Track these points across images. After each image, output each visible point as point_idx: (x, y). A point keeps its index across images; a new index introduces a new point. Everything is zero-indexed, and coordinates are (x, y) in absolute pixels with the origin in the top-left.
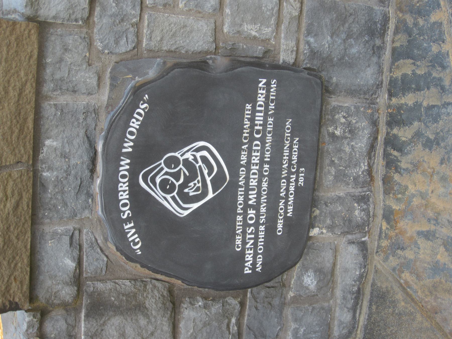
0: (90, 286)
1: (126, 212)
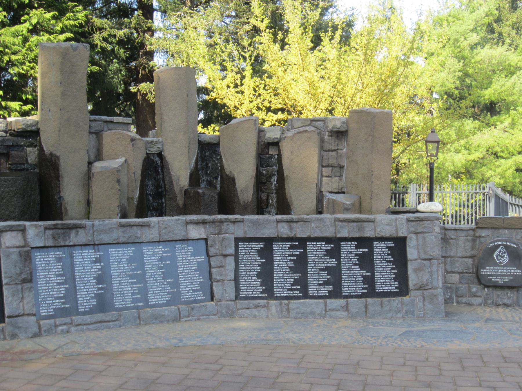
0: (478, 239)
1: (496, 244)
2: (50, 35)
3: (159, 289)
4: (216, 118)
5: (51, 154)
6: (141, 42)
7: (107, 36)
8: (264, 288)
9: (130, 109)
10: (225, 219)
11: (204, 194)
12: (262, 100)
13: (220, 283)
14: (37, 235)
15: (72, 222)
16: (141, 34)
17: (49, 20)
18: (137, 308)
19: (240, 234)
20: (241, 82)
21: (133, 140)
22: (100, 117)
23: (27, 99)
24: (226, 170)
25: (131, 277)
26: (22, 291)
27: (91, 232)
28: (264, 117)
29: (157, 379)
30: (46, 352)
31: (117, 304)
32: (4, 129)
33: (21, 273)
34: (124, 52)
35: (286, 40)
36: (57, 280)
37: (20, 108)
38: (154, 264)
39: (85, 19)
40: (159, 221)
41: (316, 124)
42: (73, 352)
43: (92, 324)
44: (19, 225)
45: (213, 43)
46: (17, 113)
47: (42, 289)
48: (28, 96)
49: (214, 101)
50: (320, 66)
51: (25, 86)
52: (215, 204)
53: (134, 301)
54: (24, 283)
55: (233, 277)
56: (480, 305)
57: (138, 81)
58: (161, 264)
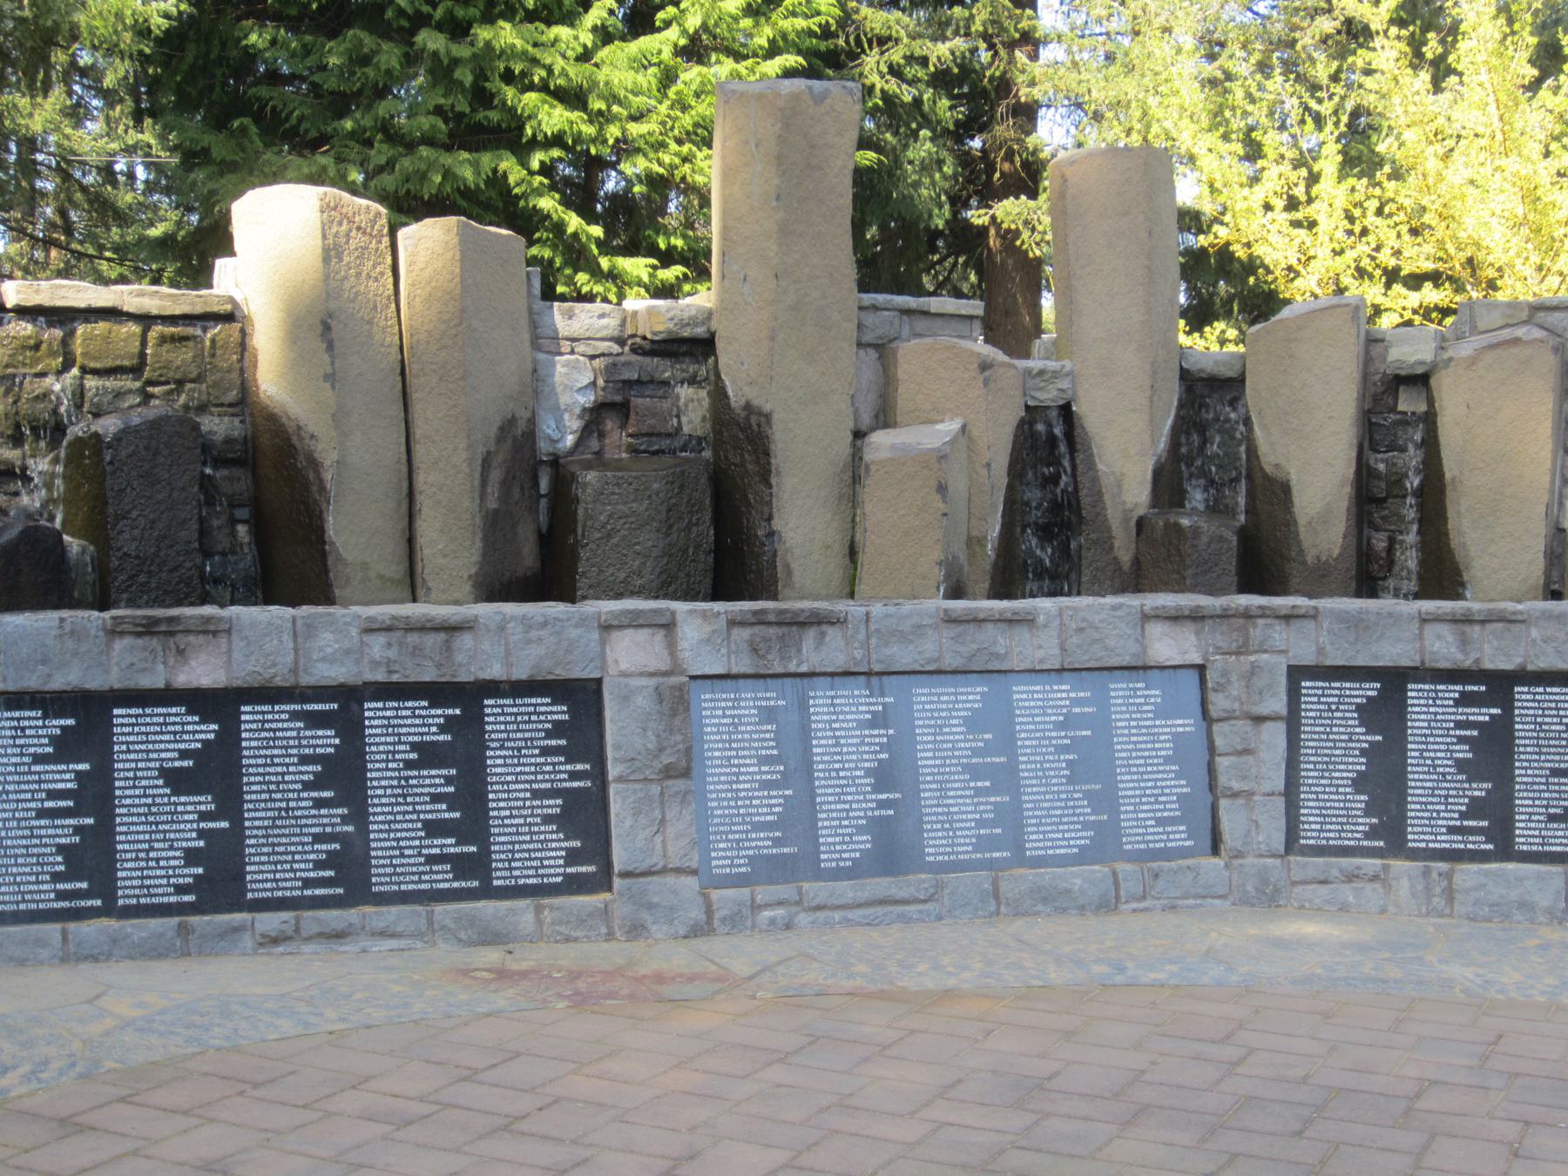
2: (737, 61)
3: (1059, 812)
4: (1223, 305)
5: (748, 407)
6: (1004, 73)
7: (902, 62)
8: (1375, 820)
9: (966, 279)
10: (1260, 607)
11: (1196, 531)
12: (1373, 245)
13: (1241, 801)
14: (708, 641)
15: (806, 605)
16: (1002, 52)
17: (736, 19)
18: (990, 865)
19: (1306, 655)
20: (1308, 193)
21: (985, 366)
22: (888, 297)
23: (671, 249)
24: (1263, 459)
25: (975, 772)
26: (662, 803)
27: (862, 636)
28: (1380, 300)
29: (1050, 1078)
30: (724, 981)
31: (931, 850)
32: (616, 333)
33: (661, 750)
34: (951, 108)
35: (1451, 59)
36: (760, 773)
37: (651, 276)
38: (1044, 738)
39: (838, 12)
40: (1061, 609)
41: (1549, 319)
42: (804, 985)
43: (859, 906)
44: (656, 611)
45: (1219, 75)
46: (642, 291)
47: (717, 799)
48: (673, 241)
49: (1224, 252)
50: (1557, 138)
51: (663, 211)
52: (1230, 563)
53: (982, 844)
54: (669, 777)
55: (1279, 784)
57: (988, 195)
58: (1066, 737)
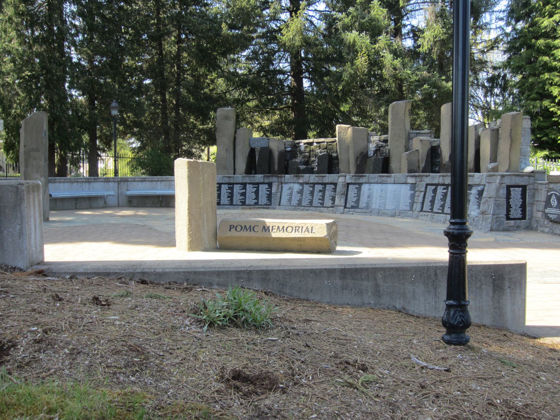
56: (548, 233)
